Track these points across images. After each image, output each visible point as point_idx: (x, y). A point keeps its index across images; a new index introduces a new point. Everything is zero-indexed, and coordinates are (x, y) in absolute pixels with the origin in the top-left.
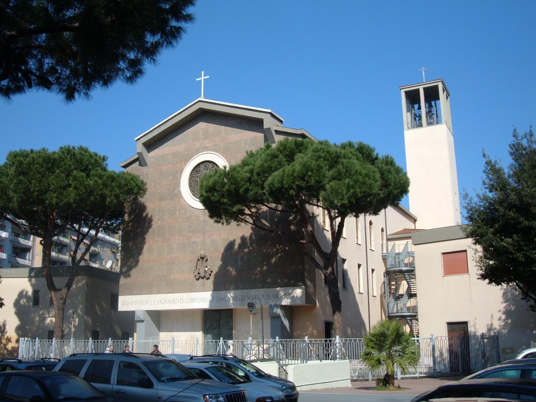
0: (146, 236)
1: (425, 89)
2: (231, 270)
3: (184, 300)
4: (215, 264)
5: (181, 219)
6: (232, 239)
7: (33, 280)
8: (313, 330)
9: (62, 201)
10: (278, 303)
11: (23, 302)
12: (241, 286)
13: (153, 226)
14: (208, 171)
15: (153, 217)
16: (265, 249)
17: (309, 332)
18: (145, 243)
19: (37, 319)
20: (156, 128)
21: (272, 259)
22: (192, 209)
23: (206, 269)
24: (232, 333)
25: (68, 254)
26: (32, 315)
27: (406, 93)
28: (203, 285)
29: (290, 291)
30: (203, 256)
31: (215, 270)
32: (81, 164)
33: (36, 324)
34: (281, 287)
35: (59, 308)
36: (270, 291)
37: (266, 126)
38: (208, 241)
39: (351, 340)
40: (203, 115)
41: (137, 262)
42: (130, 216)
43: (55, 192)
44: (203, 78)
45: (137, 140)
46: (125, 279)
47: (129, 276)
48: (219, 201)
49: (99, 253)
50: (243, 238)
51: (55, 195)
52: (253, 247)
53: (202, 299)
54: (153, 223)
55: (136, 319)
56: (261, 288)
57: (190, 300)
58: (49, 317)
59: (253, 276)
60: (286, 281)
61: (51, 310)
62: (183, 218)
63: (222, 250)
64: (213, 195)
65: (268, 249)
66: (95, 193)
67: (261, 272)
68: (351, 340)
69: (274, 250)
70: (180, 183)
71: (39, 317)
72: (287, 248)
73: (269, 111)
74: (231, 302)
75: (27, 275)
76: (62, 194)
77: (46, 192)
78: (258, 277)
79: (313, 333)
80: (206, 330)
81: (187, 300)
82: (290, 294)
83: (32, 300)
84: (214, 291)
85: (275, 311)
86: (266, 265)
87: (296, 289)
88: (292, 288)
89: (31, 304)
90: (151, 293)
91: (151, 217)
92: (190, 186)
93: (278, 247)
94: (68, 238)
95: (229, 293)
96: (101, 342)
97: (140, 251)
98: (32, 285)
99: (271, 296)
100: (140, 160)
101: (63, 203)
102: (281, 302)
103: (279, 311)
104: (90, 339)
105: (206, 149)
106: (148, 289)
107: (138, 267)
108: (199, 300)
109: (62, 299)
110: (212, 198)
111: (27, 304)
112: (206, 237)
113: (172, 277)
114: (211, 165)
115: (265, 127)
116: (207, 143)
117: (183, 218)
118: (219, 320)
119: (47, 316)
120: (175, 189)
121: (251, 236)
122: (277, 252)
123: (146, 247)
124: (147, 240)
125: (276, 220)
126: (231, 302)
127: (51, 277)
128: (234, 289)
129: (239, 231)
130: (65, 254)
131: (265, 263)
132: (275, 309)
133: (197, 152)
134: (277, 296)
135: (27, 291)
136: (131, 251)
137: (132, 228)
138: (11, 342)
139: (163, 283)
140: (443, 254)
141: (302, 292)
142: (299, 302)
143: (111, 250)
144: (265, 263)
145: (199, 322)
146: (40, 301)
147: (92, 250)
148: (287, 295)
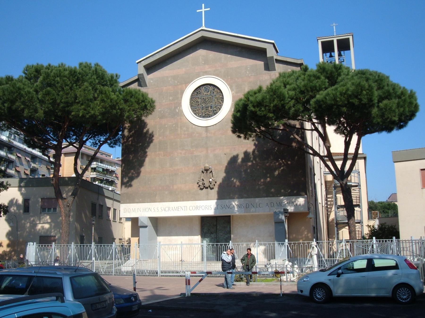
0: (147, 150)
1: (338, 41)
2: (235, 181)
3: (188, 207)
4: (219, 176)
5: (183, 136)
6: (235, 154)
7: (23, 189)
8: (308, 234)
9: (89, 113)
11: (14, 209)
13: (154, 141)
14: (209, 93)
15: (154, 133)
16: (267, 163)
17: (304, 235)
18: (147, 156)
19: (28, 225)
21: (275, 171)
22: (194, 126)
23: (211, 180)
24: (231, 236)
25: (14, 169)
26: (23, 221)
27: (322, 43)
28: (208, 194)
29: (293, 200)
30: (208, 168)
31: (219, 181)
32: (102, 79)
33: (27, 230)
34: (285, 196)
35: (66, 214)
36: (274, 199)
37: (269, 55)
39: (214, 245)
41: (138, 174)
42: (130, 131)
43: (82, 104)
44: (203, 10)
45: (138, 63)
46: (126, 189)
47: (131, 186)
48: (265, 116)
49: (38, 169)
51: (83, 107)
52: (256, 161)
53: (208, 207)
55: (140, 224)
56: (264, 197)
57: (194, 207)
58: (40, 223)
59: (257, 187)
60: (290, 191)
61: (41, 217)
62: (185, 134)
63: (225, 163)
64: (260, 111)
65: (271, 163)
66: (117, 107)
67: (264, 183)
68: (354, 242)
69: (277, 164)
70: (181, 103)
71: (30, 223)
72: (289, 163)
73: (273, 42)
74: (236, 209)
75: (17, 185)
76: (90, 107)
77: (72, 104)
78: (261, 187)
79: (308, 237)
80: (204, 236)
82: (293, 203)
83: (22, 207)
84: (218, 199)
85: (280, 217)
87: (299, 198)
88: (295, 197)
89: (22, 211)
90: (154, 201)
91: (152, 133)
92: (191, 106)
93: (281, 161)
94: (14, 155)
95: (234, 202)
96: (87, 246)
97: (141, 164)
98: (22, 194)
99: (275, 204)
100: (140, 81)
101: (89, 114)
103: (283, 217)
104: (93, 243)
105: (206, 73)
106: (151, 197)
107: (139, 178)
109: (69, 206)
110: (258, 113)
111: (17, 211)
112: (209, 151)
113: (175, 187)
114: (211, 88)
115: (268, 56)
116: (207, 68)
117: (185, 134)
119: (38, 222)
120: (176, 108)
121: (254, 151)
123: (147, 160)
124: (148, 153)
125: (278, 137)
126: (236, 209)
127: (59, 186)
128: (238, 198)
129: (247, 145)
130: (11, 169)
131: (268, 175)
132: (280, 215)
133: (198, 75)
135: (17, 200)
136: (132, 163)
137: (132, 142)
138: (2, 246)
139: (166, 193)
140: (422, 170)
141: (305, 201)
142: (302, 209)
143: (47, 167)
145: (197, 227)
146: (31, 209)
147: (33, 167)
148: (291, 203)
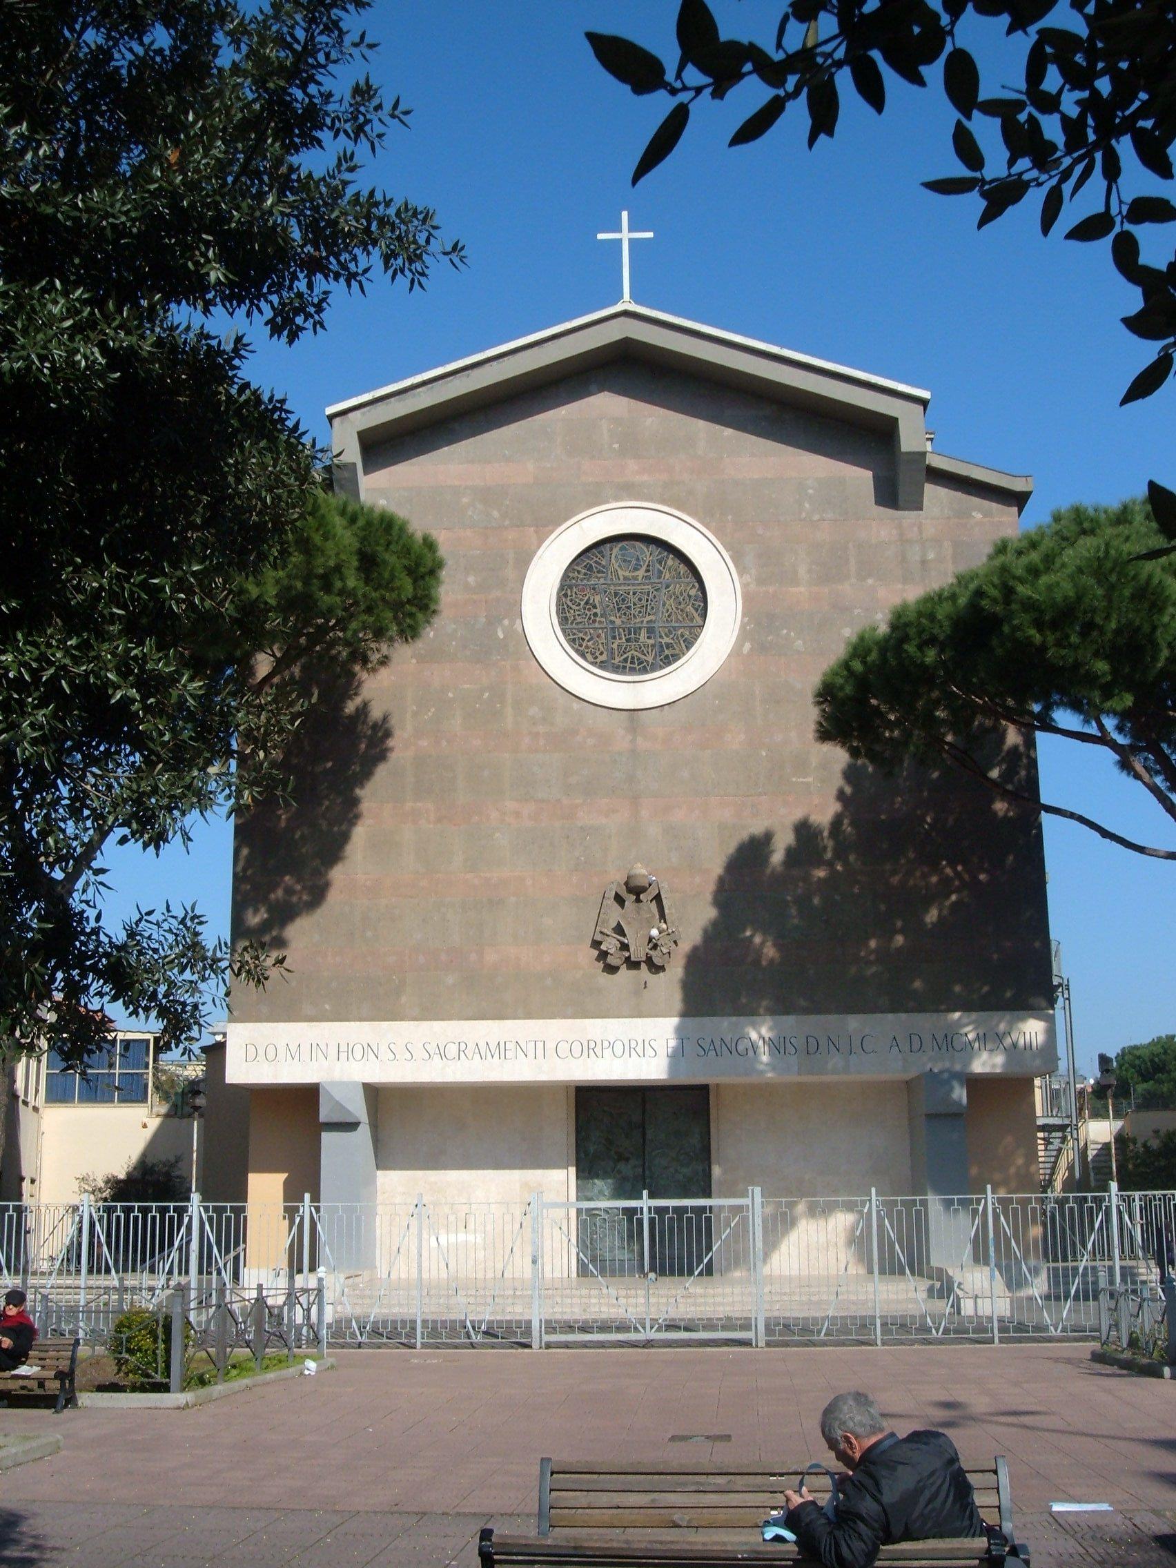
2: (757, 940)
4: (693, 917)
5: (527, 740)
10: (958, 1067)
12: (803, 1003)
13: (393, 756)
14: (641, 573)
17: (1012, 1170)
18: (357, 817)
20: (424, 383)
21: (927, 910)
22: (576, 705)
29: (1002, 1027)
34: (967, 1007)
36: (924, 1022)
38: (653, 830)
40: (631, 367)
41: (318, 894)
44: (625, 236)
45: (331, 418)
50: (804, 830)
52: (846, 863)
54: (391, 743)
57: (577, 1048)
60: (986, 989)
63: (716, 866)
64: (1059, 644)
69: (934, 879)
72: (982, 877)
74: (765, 1058)
81: (564, 1047)
82: (1000, 1038)
84: (684, 1014)
86: (902, 931)
87: (1023, 1019)
88: (1008, 1016)
91: (385, 718)
93: (948, 871)
95: (755, 1026)
97: (332, 849)
99: (282, 1051)
102: (968, 1062)
108: (618, 1048)
112: (644, 813)
113: (491, 957)
114: (648, 554)
116: (632, 469)
118: (643, 1127)
121: (836, 823)
122: (946, 886)
123: (360, 833)
124: (365, 806)
128: (772, 1012)
134: (949, 1041)
139: (450, 980)
144: (899, 924)
145: (562, 1132)
148: (990, 1039)
